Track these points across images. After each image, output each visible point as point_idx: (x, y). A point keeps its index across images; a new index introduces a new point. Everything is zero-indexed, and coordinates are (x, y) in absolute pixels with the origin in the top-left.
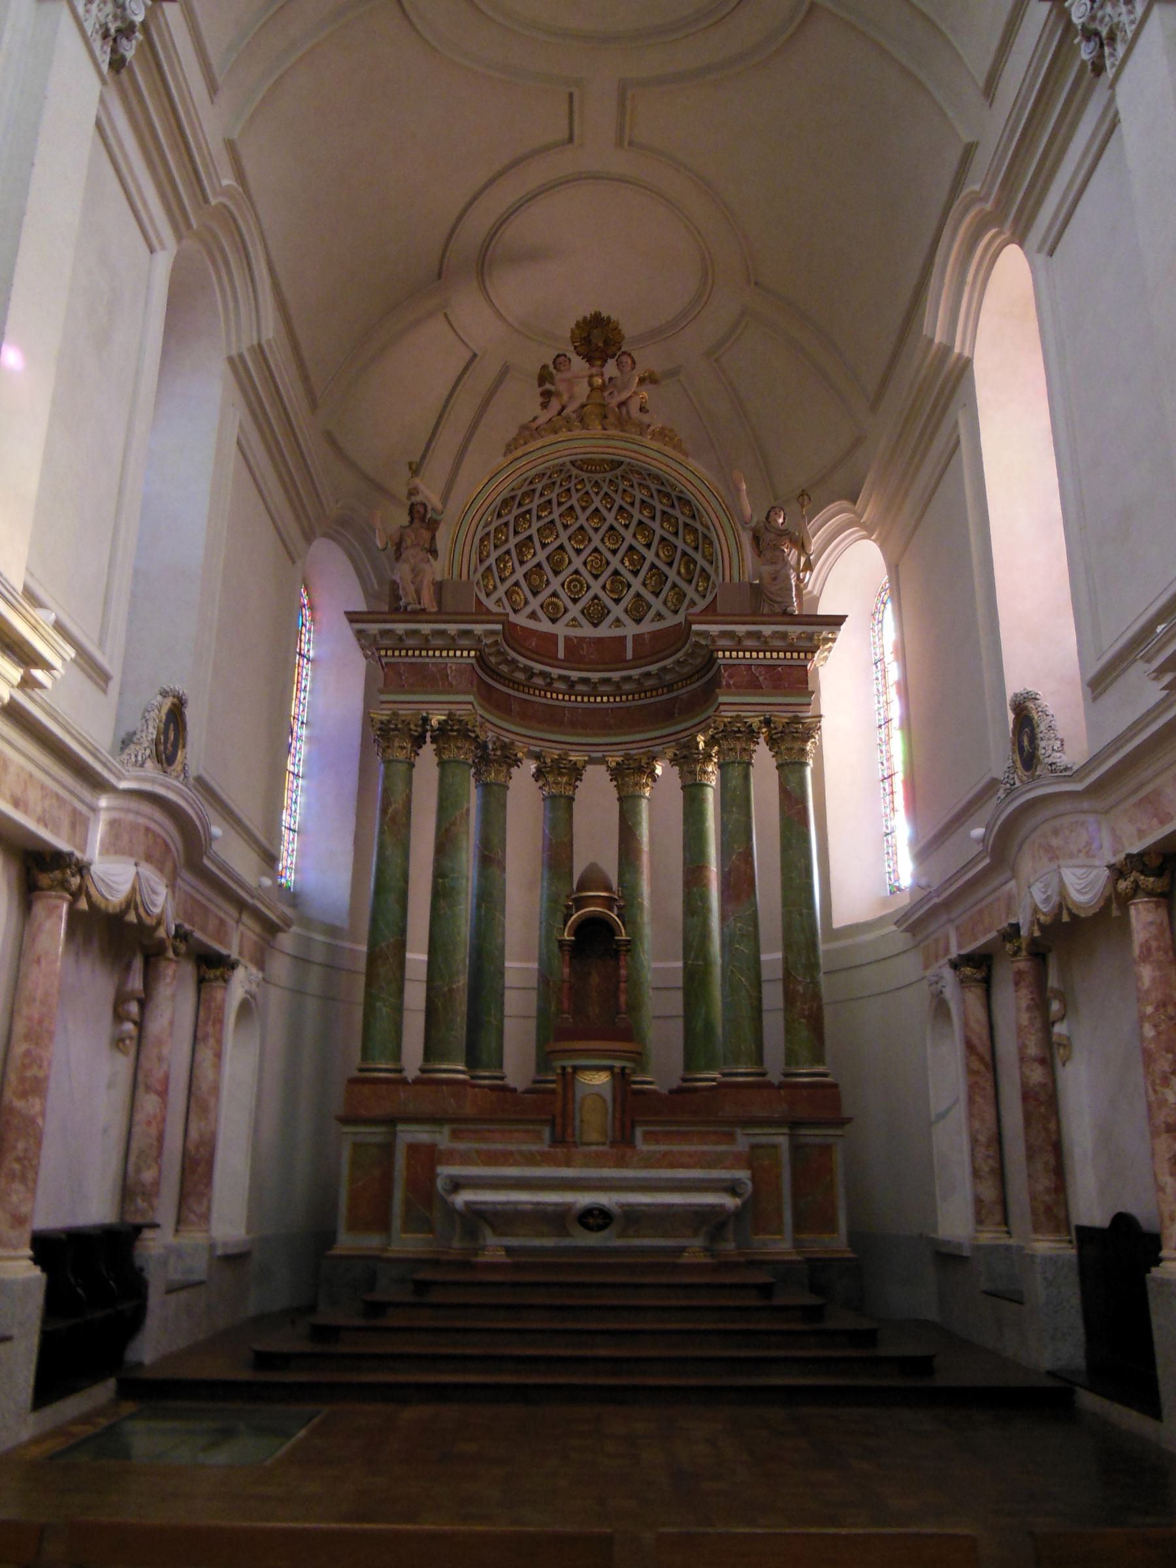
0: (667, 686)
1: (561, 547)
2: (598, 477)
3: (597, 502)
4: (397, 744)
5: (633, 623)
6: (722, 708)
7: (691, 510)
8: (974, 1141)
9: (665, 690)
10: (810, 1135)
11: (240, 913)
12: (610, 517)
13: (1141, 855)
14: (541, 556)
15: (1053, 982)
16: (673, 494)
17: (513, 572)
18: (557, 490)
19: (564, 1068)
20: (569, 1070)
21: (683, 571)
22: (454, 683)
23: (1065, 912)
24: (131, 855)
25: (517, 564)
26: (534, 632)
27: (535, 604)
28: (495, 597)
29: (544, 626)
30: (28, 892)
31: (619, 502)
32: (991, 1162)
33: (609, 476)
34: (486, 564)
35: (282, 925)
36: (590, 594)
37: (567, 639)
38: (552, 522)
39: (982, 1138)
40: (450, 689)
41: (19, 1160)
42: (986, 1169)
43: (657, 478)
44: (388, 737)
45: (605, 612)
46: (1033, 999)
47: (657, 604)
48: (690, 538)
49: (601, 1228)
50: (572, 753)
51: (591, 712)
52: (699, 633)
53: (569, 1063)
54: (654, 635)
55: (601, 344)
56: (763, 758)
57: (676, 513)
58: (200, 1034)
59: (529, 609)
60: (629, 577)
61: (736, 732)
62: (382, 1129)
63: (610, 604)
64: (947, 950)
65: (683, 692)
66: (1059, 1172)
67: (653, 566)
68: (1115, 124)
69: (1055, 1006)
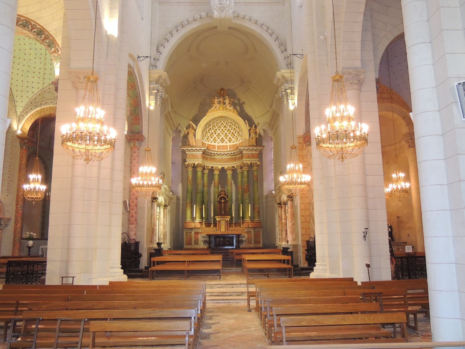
14: (213, 131)
27: (212, 140)
29: (213, 144)
40: (198, 159)
47: (233, 139)
51: (222, 159)
54: (233, 145)
62: (198, 194)
65: (238, 156)
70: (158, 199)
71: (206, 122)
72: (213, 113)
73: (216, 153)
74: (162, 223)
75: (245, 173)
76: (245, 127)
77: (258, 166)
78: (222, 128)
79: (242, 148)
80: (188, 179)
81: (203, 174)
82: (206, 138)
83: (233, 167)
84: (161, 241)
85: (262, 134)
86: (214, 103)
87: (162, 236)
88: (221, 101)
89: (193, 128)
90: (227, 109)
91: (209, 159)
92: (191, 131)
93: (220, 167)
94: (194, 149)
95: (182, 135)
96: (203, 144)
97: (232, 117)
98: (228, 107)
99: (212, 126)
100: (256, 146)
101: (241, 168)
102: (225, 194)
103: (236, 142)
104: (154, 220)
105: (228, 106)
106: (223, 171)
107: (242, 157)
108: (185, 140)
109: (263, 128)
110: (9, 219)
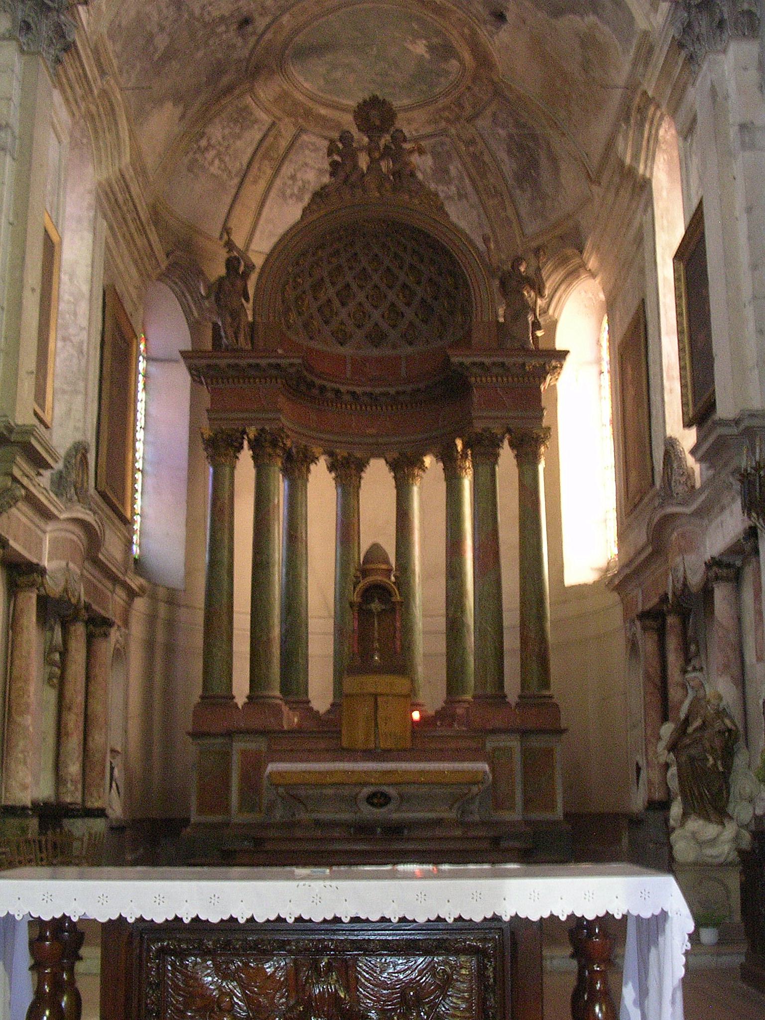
3: (376, 249)
10: (537, 742)
11: (114, 585)
12: (387, 262)
30: (13, 590)
41: (22, 752)
44: (216, 445)
45: (383, 336)
49: (381, 806)
55: (378, 123)
56: (507, 456)
69: (693, 648)
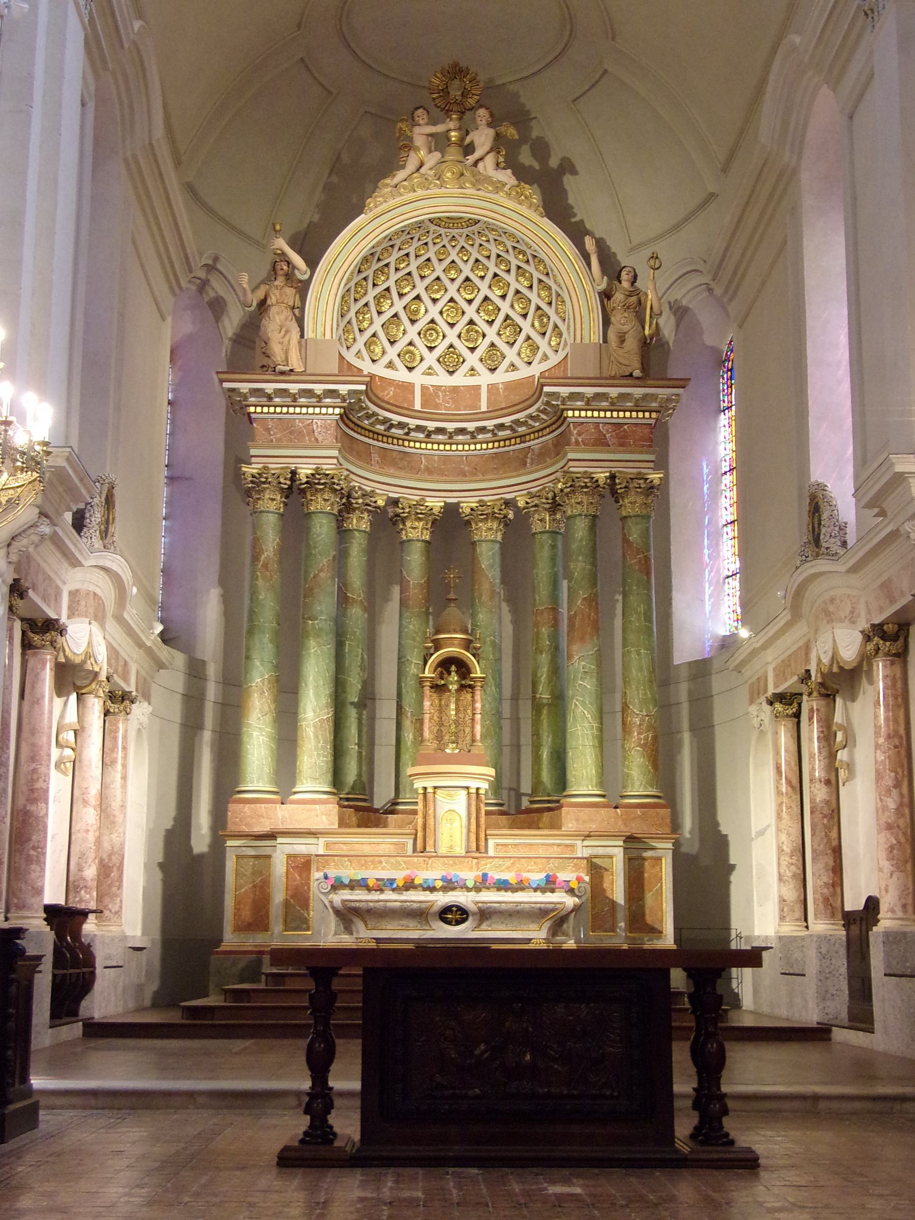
0: (520, 437)
1: (418, 297)
2: (455, 232)
3: (453, 255)
4: (267, 496)
5: (488, 372)
6: (571, 464)
7: (545, 268)
8: (780, 850)
9: (518, 440)
13: (881, 625)
14: (399, 305)
15: (838, 718)
16: (528, 252)
17: (371, 323)
18: (416, 244)
19: (425, 788)
20: (430, 790)
21: (537, 324)
22: (320, 439)
23: (835, 665)
24: (87, 617)
25: (375, 314)
26: (390, 382)
27: (392, 353)
28: (354, 350)
29: (401, 375)
31: (475, 255)
32: (793, 868)
33: (466, 231)
34: (346, 319)
35: (167, 664)
36: (446, 343)
37: (424, 388)
38: (409, 274)
39: (787, 849)
42: (789, 874)
43: (512, 235)
46: (822, 732)
48: (543, 294)
49: (458, 923)
50: (428, 499)
51: (446, 459)
52: (549, 394)
53: (429, 783)
54: (510, 386)
57: (530, 268)
58: (107, 760)
59: (385, 360)
60: (484, 327)
61: (583, 487)
63: (466, 353)
64: (766, 691)
65: (535, 443)
66: (837, 870)
67: (507, 317)
68: (871, 76)
69: (840, 736)
70: (62, 631)
71: (364, 247)
72: (412, 197)
73: (413, 423)
74: (94, 789)
75: (581, 528)
76: (579, 283)
77: (651, 489)
78: (452, 292)
79: (564, 391)
80: (255, 558)
81: (342, 533)
82: (362, 340)
83: (508, 503)
84: (87, 900)
85: (667, 325)
86: (409, 146)
87: (91, 872)
88: (446, 135)
89: (289, 277)
90: (479, 181)
91: (376, 457)
92: (281, 295)
93: (435, 503)
94: (294, 388)
95: (232, 323)
96: (347, 370)
97: (510, 225)
98: (488, 166)
99: (394, 277)
100: (641, 381)
101: (555, 506)
102: (467, 645)
103: (520, 369)
104: (33, 759)
105: (490, 160)
106: (451, 525)
107: (560, 445)
108: (248, 348)
109: (676, 295)
110: (39, 958)
